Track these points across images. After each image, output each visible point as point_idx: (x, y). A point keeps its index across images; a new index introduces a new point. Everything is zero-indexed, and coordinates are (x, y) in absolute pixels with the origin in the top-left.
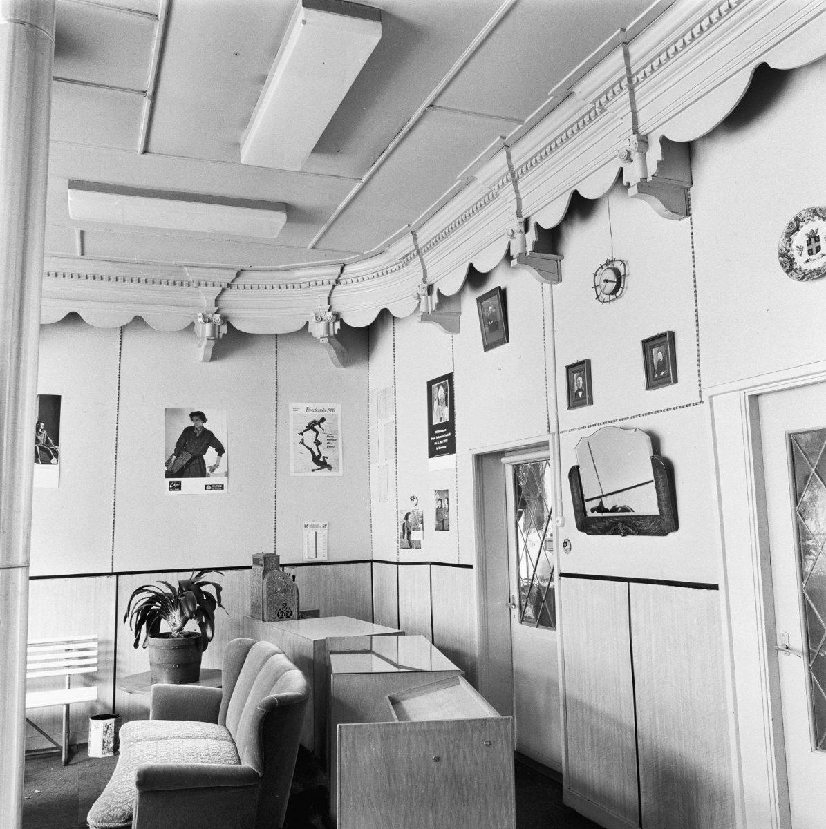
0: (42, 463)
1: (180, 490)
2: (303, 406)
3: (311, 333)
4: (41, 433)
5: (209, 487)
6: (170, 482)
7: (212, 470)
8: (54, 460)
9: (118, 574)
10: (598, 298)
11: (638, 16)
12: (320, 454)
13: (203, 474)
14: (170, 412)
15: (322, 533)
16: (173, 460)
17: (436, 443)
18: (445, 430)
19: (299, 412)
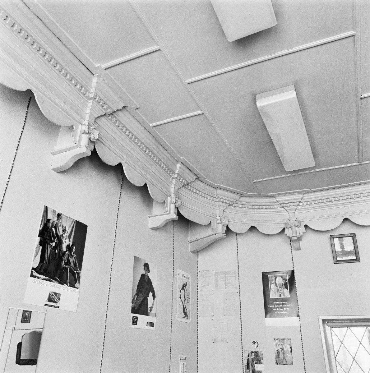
0: (70, 286)
6: (133, 317)
7: (151, 311)
8: (77, 285)
13: (146, 313)
14: (136, 259)
16: (135, 299)
19: (181, 276)
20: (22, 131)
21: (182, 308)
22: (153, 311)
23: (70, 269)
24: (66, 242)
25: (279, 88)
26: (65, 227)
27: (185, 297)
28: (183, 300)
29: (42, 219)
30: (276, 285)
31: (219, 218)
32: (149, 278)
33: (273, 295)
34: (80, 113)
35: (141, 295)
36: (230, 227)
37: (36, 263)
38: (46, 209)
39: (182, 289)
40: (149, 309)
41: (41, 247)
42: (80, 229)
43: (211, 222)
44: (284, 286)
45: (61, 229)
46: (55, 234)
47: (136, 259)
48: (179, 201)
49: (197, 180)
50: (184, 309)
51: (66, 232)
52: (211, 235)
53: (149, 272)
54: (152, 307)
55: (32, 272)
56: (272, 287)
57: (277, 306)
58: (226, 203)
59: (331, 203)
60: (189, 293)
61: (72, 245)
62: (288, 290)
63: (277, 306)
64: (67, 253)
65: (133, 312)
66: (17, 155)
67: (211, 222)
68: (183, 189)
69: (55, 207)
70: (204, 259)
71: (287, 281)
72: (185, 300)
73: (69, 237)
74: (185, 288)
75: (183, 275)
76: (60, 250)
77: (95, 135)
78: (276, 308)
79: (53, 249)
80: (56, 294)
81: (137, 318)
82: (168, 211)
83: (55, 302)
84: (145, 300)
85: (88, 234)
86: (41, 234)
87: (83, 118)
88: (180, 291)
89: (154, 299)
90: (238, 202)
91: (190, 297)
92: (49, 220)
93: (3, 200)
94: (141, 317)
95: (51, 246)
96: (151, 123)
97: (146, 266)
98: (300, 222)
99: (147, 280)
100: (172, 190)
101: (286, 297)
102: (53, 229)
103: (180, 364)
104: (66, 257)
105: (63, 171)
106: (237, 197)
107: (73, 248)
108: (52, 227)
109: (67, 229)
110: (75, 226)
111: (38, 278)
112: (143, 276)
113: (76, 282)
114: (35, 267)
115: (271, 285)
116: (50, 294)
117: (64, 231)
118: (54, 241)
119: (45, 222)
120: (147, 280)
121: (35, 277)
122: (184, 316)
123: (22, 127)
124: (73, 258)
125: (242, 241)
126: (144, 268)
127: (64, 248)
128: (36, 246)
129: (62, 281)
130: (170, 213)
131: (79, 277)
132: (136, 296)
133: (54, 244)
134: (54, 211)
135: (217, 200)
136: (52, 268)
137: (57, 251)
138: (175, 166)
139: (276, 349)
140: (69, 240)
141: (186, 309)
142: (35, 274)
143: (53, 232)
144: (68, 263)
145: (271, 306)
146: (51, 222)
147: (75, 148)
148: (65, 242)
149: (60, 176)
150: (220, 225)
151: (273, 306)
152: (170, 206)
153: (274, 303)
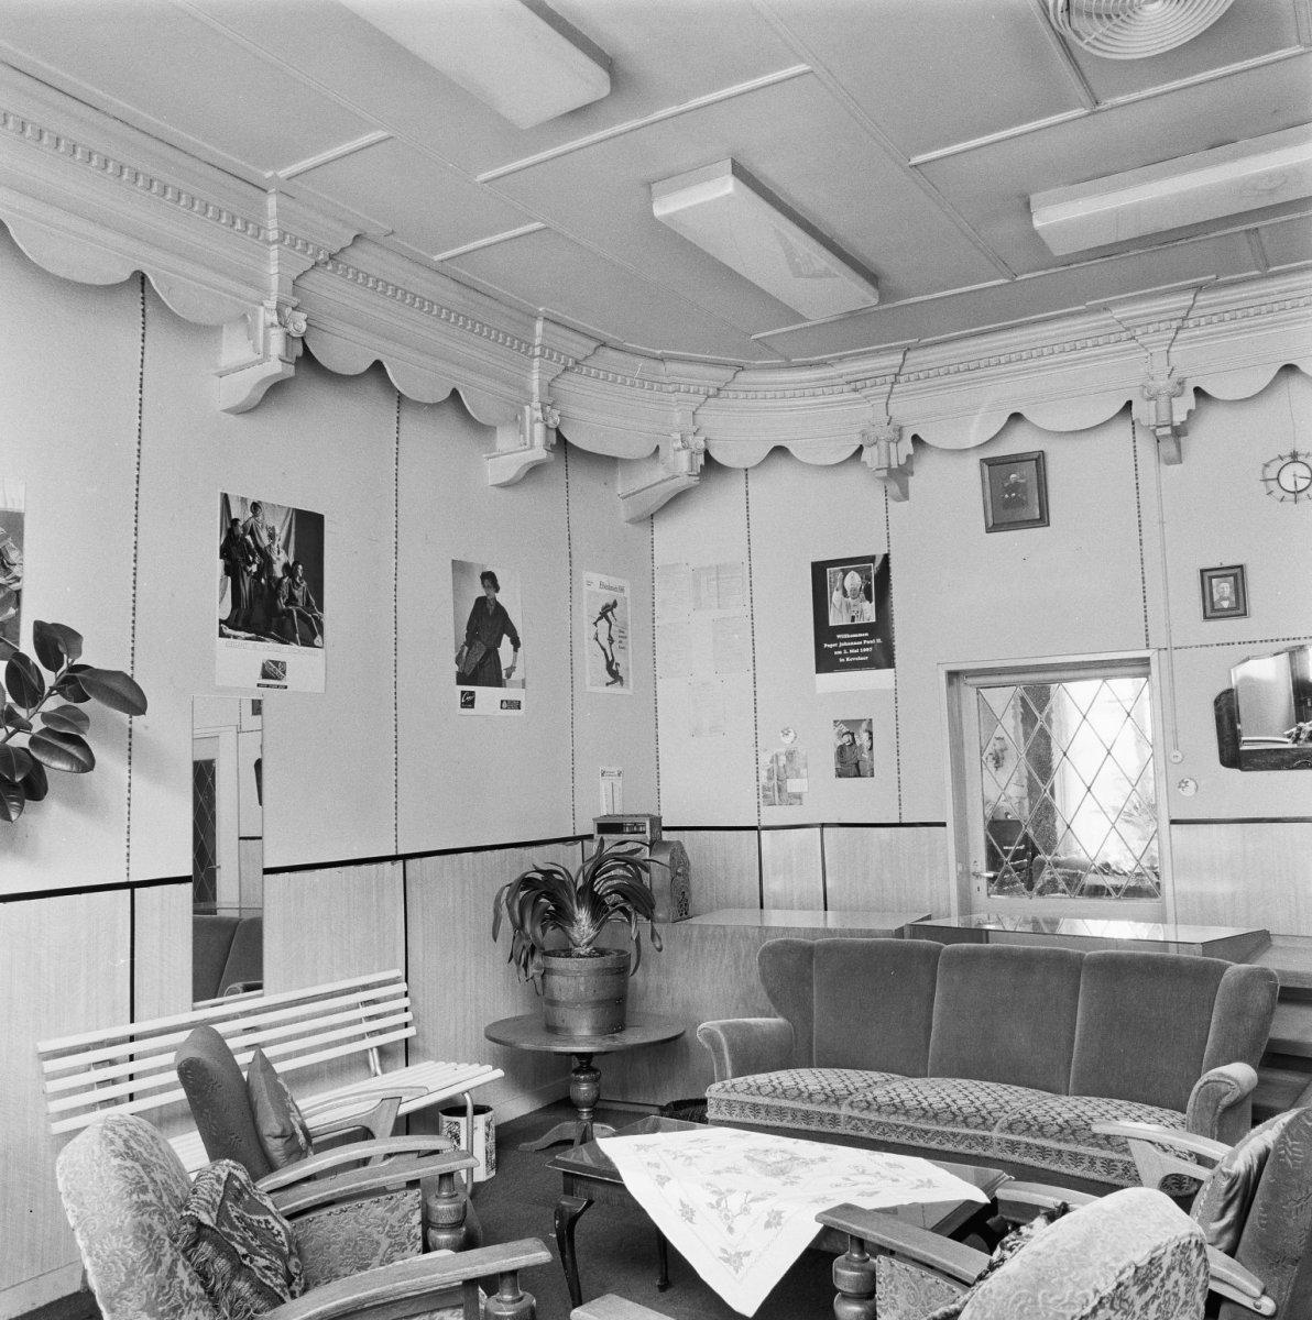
0: (302, 645)
1: (473, 707)
2: (596, 578)
3: (865, 462)
4: (298, 585)
5: (505, 705)
6: (463, 693)
7: (509, 676)
8: (318, 640)
9: (405, 857)
10: (1266, 466)
11: (1195, 73)
12: (613, 660)
13: (498, 682)
14: (459, 567)
15: (619, 783)
16: (464, 654)
17: (842, 660)
18: (867, 634)
19: (594, 587)
20: (143, 348)
21: (605, 662)
22: (514, 676)
23: (298, 612)
24: (281, 559)
25: (694, 172)
26: (273, 529)
27: (610, 635)
28: (606, 644)
29: (221, 523)
30: (845, 593)
31: (678, 437)
32: (498, 606)
33: (835, 619)
34: (255, 282)
35: (478, 643)
36: (715, 454)
37: (225, 610)
38: (225, 498)
39: (599, 619)
40: (504, 673)
41: (229, 578)
42: (309, 526)
43: (658, 447)
44: (862, 595)
45: (264, 534)
46: (253, 546)
47: (459, 567)
48: (556, 413)
49: (602, 350)
50: (609, 665)
51: (277, 538)
52: (663, 481)
53: (497, 589)
54: (511, 669)
55: (221, 629)
56: (836, 597)
57: (845, 644)
58: (697, 393)
59: (978, 373)
60: (626, 624)
61: (295, 563)
62: (873, 603)
63: (845, 644)
64: (285, 580)
65: (460, 682)
66: (142, 451)
67: (658, 447)
68: (567, 376)
69: (244, 489)
70: (670, 537)
71: (870, 580)
72: (611, 644)
73: (286, 547)
74: (609, 614)
75: (602, 585)
76: (271, 578)
77: (299, 324)
78: (842, 649)
79: (254, 577)
80: (276, 663)
81: (472, 693)
82: (528, 442)
83: (276, 678)
84: (492, 654)
85: (330, 532)
86: (225, 552)
87: (267, 291)
88: (595, 624)
89: (516, 650)
90: (731, 386)
91: (629, 633)
92: (236, 521)
93: (136, 529)
94: (481, 692)
95: (249, 573)
96: (437, 251)
97: (489, 579)
98: (900, 430)
99: (491, 609)
100: (535, 387)
101: (866, 621)
102: (248, 537)
103: (604, 784)
104: (285, 590)
105: (246, 410)
106: (728, 374)
107: (297, 568)
108: (244, 535)
109: (277, 531)
110: (294, 522)
111: (235, 637)
112: (481, 602)
113: (315, 636)
114: (225, 617)
115: (831, 593)
116: (264, 665)
117: (272, 536)
118: (254, 562)
119: (229, 526)
120: (491, 609)
121: (228, 636)
122: (610, 679)
123: (140, 337)
124: (301, 588)
125: (760, 487)
126: (483, 583)
127: (278, 572)
128: (219, 578)
129: (285, 638)
130: (532, 447)
131: (320, 625)
132: (466, 648)
133: (254, 568)
134: (244, 500)
135: (671, 388)
136: (259, 615)
137: (263, 581)
138: (532, 328)
139: (839, 743)
140: (287, 552)
141: (617, 664)
142: (228, 631)
143: (249, 545)
144: (292, 600)
145: (831, 646)
146: (241, 524)
147: (260, 362)
148: (279, 559)
149: (240, 420)
150: (684, 455)
151: (835, 645)
152: (532, 430)
153: (839, 636)
